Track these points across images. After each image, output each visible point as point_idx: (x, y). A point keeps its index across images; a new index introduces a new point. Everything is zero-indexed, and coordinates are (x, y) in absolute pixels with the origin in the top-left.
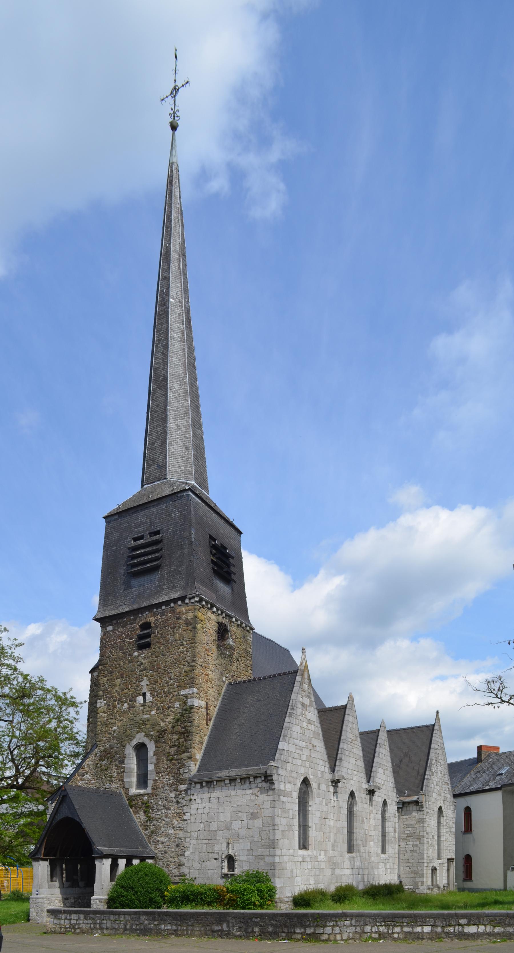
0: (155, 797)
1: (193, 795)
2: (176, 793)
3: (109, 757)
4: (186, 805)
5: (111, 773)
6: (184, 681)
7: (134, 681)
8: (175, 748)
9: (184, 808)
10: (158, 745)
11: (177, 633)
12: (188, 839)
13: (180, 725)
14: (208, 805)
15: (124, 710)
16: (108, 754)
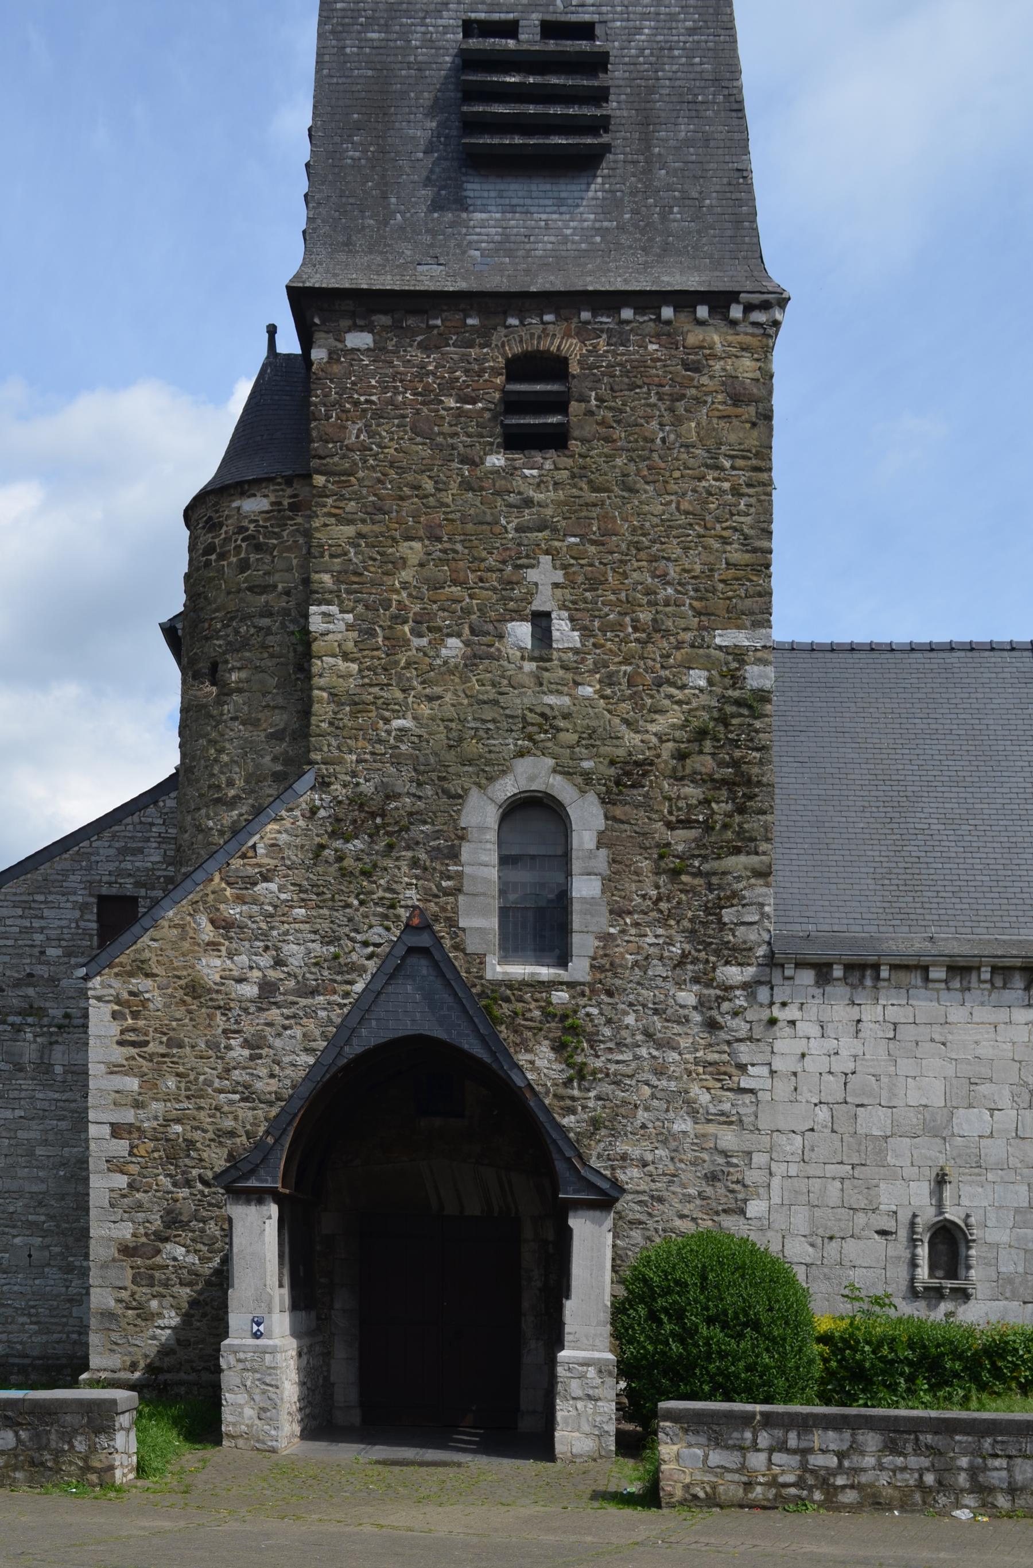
0: (604, 997)
1: (784, 1004)
2: (706, 992)
3: (384, 825)
4: (750, 1039)
5: (389, 889)
6: (729, 598)
7: (491, 561)
8: (693, 833)
9: (742, 1047)
10: (618, 811)
11: (690, 420)
12: (758, 1159)
13: (713, 754)
14: (848, 1045)
15: (446, 663)
16: (373, 815)
